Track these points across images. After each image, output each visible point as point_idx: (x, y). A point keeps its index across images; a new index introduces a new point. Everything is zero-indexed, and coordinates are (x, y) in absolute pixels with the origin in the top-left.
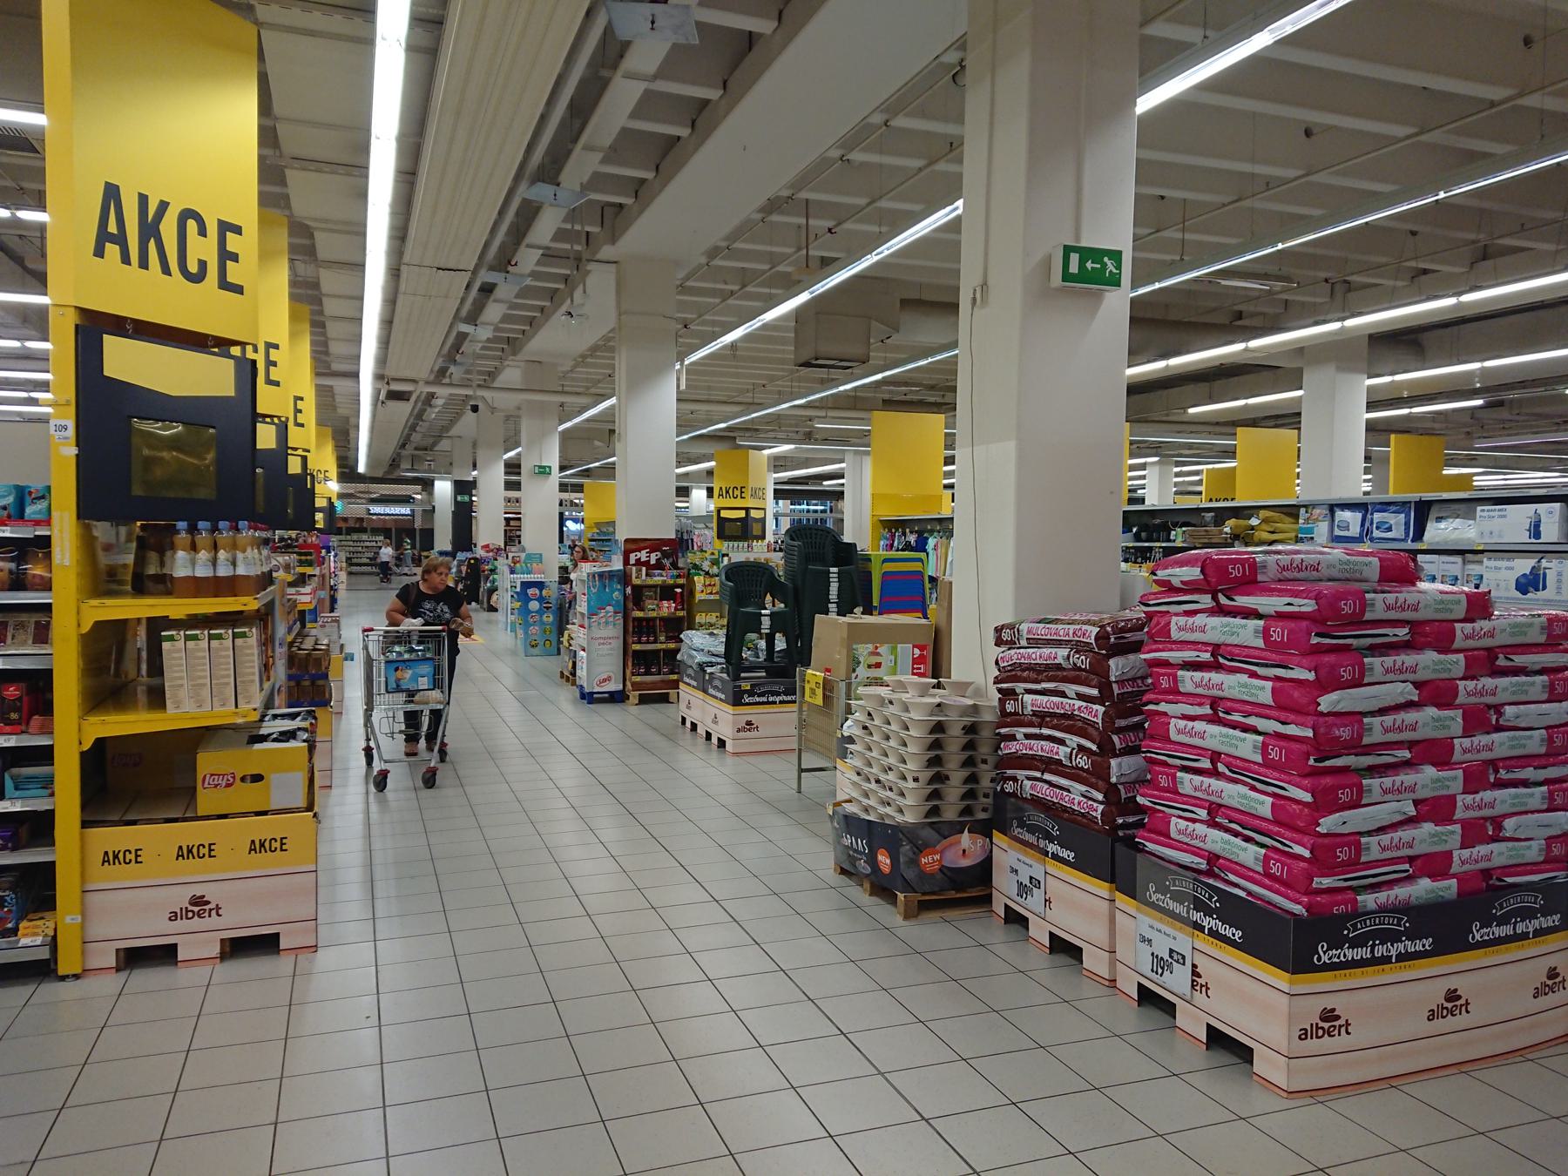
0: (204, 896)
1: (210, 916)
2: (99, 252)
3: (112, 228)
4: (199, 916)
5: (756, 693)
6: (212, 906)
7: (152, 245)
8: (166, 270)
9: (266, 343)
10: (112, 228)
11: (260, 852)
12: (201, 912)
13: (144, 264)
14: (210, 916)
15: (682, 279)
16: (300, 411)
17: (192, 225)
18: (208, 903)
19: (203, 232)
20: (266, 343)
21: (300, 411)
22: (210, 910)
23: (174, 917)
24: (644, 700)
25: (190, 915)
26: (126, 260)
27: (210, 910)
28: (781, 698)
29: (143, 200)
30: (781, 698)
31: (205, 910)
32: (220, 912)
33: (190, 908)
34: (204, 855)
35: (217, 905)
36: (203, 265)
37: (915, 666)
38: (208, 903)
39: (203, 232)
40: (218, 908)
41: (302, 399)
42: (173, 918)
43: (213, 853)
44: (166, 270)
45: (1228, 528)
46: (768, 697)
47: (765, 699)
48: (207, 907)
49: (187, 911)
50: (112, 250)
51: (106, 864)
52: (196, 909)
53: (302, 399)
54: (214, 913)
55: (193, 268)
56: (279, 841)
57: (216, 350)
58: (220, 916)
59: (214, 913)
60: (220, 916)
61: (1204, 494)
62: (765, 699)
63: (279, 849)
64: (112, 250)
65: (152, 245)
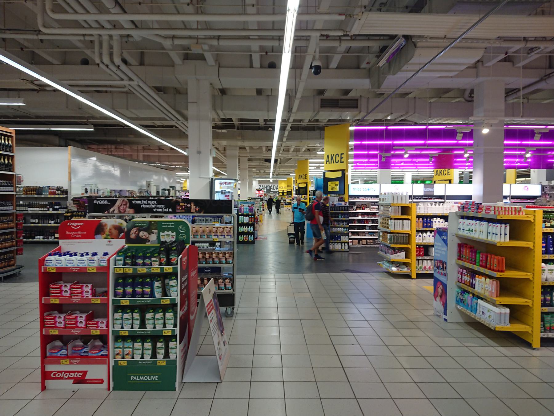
2: (326, 163)
7: (332, 160)
8: (334, 163)
10: (328, 160)
11: (331, 163)
16: (343, 158)
17: (337, 156)
29: (331, 155)
34: (446, 174)
39: (338, 156)
43: (449, 174)
50: (328, 162)
51: (437, 175)
55: (337, 161)
56: (340, 155)
63: (447, 174)
64: (328, 162)
65: (332, 160)
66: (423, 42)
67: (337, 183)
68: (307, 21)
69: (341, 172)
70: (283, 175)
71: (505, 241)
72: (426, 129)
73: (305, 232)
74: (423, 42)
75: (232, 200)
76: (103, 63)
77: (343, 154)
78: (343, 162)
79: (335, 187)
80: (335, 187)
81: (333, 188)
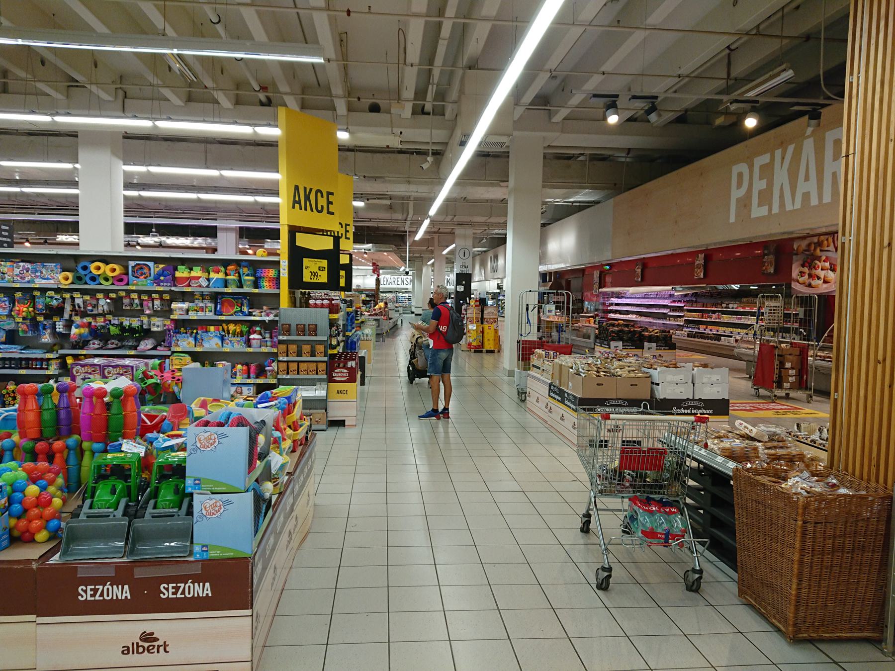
0: (153, 634)
1: (158, 652)
2: (293, 207)
3: (297, 199)
4: (148, 651)
5: (682, 407)
6: (160, 643)
7: (308, 203)
8: (312, 210)
9: (327, 192)
10: (297, 199)
12: (151, 648)
13: (306, 209)
14: (158, 652)
15: (740, 34)
16: (331, 203)
17: (319, 194)
18: (156, 640)
19: (322, 196)
20: (327, 192)
21: (331, 203)
22: (159, 646)
23: (126, 651)
24: (475, 352)
25: (141, 650)
26: (301, 209)
27: (159, 646)
28: (701, 411)
29: (305, 188)
30: (701, 411)
31: (154, 646)
32: (168, 649)
33: (141, 643)
35: (165, 642)
36: (322, 207)
37: (342, 283)
38: (156, 640)
39: (322, 196)
40: (165, 645)
41: (332, 194)
42: (126, 652)
44: (312, 210)
45: (369, 282)
46: (691, 410)
47: (689, 411)
48: (156, 644)
49: (138, 646)
50: (297, 206)
52: (146, 645)
53: (332, 194)
54: (162, 649)
55: (319, 208)
57: (411, 369)
58: (168, 652)
59: (162, 649)
60: (168, 652)
61: (257, 291)
62: (689, 411)
64: (297, 206)
65: (308, 203)
66: (807, 378)
67: (324, 263)
68: (124, 110)
69: (348, 262)
70: (45, 177)
71: (533, 366)
72: (432, 223)
73: (10, 568)
74: (807, 378)
75: (425, 101)
76: (766, 442)
77: (349, 225)
78: (333, 213)
79: (320, 273)
80: (320, 273)
81: (314, 274)
